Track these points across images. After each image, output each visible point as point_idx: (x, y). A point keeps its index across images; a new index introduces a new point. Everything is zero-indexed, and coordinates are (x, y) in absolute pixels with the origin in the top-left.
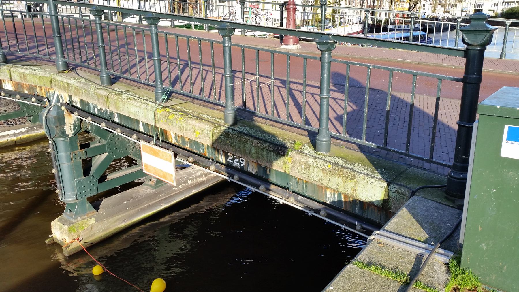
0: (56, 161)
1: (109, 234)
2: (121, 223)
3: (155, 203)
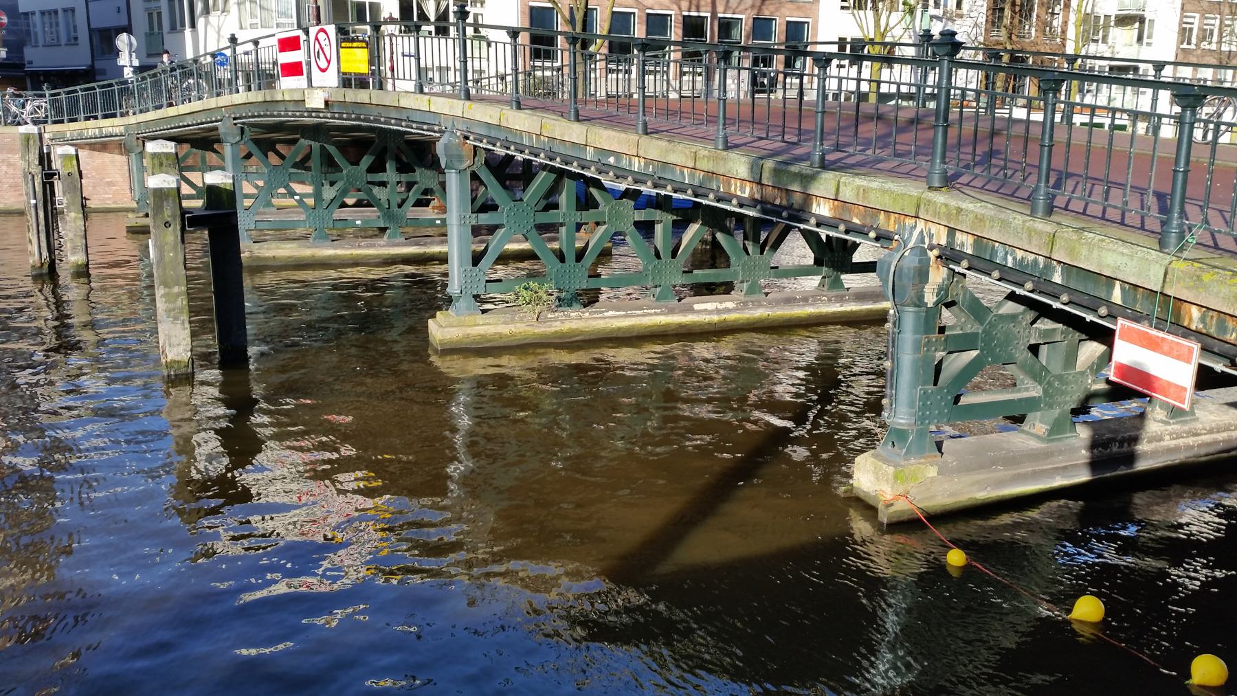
0: (893, 346)
1: (957, 506)
2: (980, 491)
3: (1046, 470)
